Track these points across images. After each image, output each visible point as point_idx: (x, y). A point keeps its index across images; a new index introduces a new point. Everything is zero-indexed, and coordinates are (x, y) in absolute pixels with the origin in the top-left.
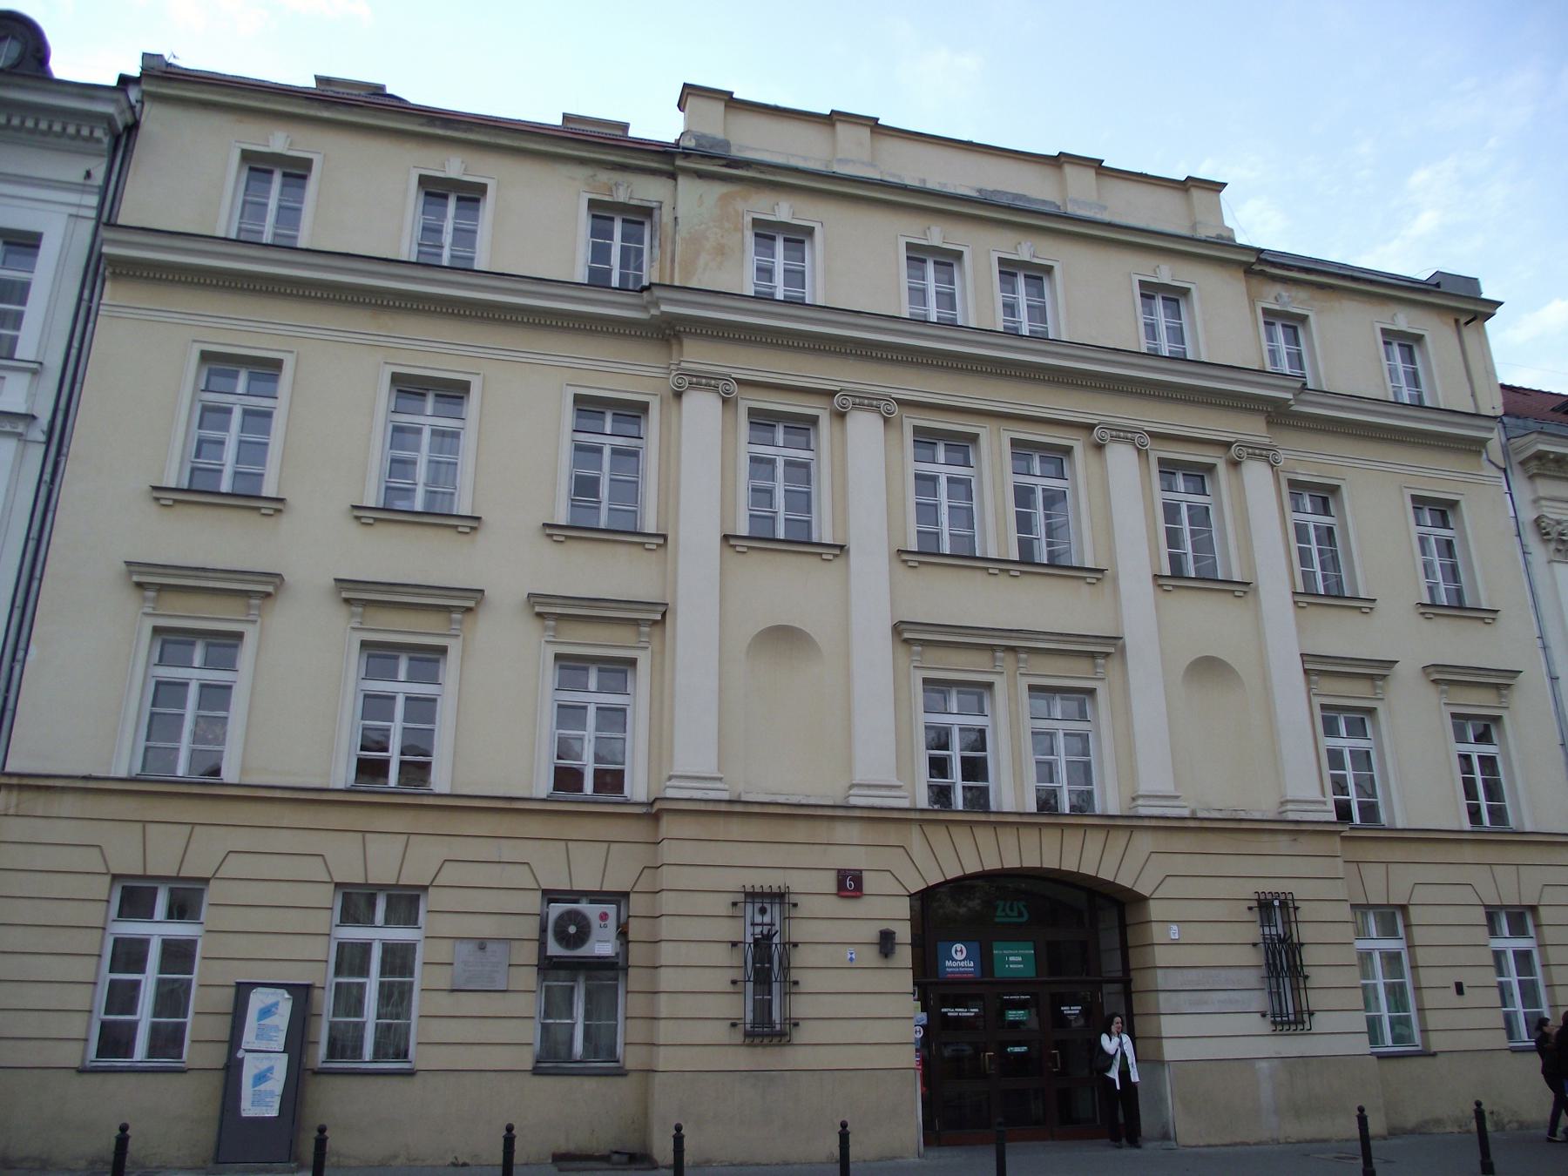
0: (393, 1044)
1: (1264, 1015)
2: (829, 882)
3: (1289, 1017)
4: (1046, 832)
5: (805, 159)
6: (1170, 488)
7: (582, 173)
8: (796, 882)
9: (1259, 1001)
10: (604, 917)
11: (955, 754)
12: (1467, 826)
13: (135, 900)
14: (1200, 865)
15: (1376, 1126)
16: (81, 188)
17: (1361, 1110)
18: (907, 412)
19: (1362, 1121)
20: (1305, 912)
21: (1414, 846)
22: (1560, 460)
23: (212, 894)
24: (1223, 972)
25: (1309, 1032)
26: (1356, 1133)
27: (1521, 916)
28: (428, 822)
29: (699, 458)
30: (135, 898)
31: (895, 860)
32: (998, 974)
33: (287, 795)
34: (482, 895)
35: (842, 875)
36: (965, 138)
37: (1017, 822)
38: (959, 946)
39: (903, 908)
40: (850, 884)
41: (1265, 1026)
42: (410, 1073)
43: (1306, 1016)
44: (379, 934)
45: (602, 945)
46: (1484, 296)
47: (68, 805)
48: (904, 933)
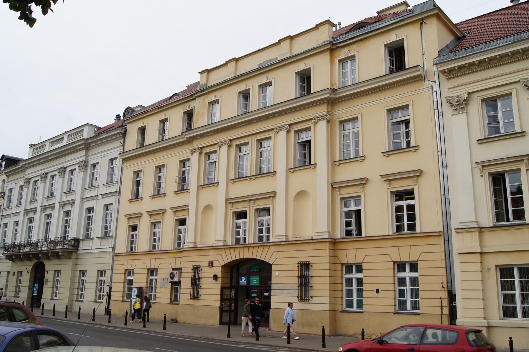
0: (360, 304)
1: (298, 297)
2: (207, 264)
3: (304, 298)
4: (250, 248)
5: (221, 78)
6: (98, 187)
8: (202, 264)
9: (297, 293)
11: (264, 228)
14: (286, 254)
17: (323, 327)
19: (323, 330)
20: (315, 267)
21: (431, 238)
23: (135, 271)
25: (309, 303)
26: (321, 333)
27: (130, 272)
28: (185, 254)
30: (401, 267)
31: (218, 258)
32: (251, 284)
33: (275, 244)
35: (209, 262)
36: (217, 65)
37: (250, 246)
38: (243, 278)
39: (220, 269)
40: (211, 264)
42: (419, 314)
43: (310, 298)
44: (408, 275)
45: (176, 279)
48: (219, 275)
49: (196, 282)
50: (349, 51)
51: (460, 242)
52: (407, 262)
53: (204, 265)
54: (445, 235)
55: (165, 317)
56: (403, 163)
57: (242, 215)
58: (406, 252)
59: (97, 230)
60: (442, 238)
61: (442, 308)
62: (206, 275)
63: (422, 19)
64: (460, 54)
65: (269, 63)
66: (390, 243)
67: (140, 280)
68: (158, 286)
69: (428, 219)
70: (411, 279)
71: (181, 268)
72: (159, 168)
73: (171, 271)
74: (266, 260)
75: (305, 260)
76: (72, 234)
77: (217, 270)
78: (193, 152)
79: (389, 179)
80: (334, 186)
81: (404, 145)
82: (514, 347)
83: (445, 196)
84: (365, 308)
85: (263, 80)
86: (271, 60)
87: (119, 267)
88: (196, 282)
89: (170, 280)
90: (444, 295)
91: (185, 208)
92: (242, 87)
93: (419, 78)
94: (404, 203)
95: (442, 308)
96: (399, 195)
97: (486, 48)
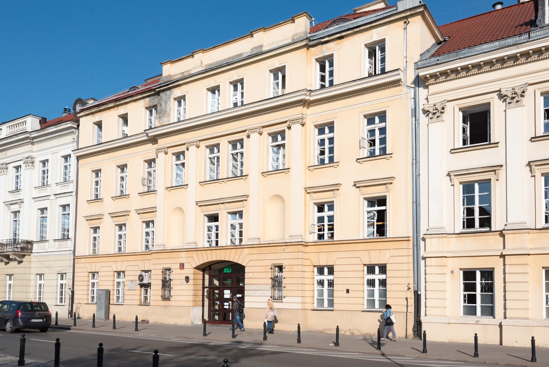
0: (331, 303)
14: (133, 263)
15: (139, 320)
18: (201, 142)
22: (548, 49)
24: (264, 286)
26: (297, 330)
35: (180, 264)
40: (182, 266)
41: (160, 298)
45: (145, 281)
49: (166, 284)
50: (328, 49)
51: (431, 247)
53: (175, 267)
54: (417, 239)
55: (137, 319)
57: (214, 218)
58: (379, 254)
59: (54, 231)
61: (407, 307)
62: (177, 277)
63: (406, 17)
64: (441, 58)
66: (361, 246)
67: (106, 282)
68: (126, 288)
69: (398, 223)
71: (150, 271)
72: (123, 168)
73: (139, 273)
74: (239, 262)
75: (278, 262)
76: (23, 236)
77: (189, 271)
78: (158, 150)
82: (479, 342)
84: (336, 307)
85: (234, 75)
86: (241, 55)
87: (80, 270)
88: (166, 284)
89: (139, 282)
91: (152, 210)
93: (396, 83)
95: (407, 307)
96: (372, 202)
97: (444, 59)
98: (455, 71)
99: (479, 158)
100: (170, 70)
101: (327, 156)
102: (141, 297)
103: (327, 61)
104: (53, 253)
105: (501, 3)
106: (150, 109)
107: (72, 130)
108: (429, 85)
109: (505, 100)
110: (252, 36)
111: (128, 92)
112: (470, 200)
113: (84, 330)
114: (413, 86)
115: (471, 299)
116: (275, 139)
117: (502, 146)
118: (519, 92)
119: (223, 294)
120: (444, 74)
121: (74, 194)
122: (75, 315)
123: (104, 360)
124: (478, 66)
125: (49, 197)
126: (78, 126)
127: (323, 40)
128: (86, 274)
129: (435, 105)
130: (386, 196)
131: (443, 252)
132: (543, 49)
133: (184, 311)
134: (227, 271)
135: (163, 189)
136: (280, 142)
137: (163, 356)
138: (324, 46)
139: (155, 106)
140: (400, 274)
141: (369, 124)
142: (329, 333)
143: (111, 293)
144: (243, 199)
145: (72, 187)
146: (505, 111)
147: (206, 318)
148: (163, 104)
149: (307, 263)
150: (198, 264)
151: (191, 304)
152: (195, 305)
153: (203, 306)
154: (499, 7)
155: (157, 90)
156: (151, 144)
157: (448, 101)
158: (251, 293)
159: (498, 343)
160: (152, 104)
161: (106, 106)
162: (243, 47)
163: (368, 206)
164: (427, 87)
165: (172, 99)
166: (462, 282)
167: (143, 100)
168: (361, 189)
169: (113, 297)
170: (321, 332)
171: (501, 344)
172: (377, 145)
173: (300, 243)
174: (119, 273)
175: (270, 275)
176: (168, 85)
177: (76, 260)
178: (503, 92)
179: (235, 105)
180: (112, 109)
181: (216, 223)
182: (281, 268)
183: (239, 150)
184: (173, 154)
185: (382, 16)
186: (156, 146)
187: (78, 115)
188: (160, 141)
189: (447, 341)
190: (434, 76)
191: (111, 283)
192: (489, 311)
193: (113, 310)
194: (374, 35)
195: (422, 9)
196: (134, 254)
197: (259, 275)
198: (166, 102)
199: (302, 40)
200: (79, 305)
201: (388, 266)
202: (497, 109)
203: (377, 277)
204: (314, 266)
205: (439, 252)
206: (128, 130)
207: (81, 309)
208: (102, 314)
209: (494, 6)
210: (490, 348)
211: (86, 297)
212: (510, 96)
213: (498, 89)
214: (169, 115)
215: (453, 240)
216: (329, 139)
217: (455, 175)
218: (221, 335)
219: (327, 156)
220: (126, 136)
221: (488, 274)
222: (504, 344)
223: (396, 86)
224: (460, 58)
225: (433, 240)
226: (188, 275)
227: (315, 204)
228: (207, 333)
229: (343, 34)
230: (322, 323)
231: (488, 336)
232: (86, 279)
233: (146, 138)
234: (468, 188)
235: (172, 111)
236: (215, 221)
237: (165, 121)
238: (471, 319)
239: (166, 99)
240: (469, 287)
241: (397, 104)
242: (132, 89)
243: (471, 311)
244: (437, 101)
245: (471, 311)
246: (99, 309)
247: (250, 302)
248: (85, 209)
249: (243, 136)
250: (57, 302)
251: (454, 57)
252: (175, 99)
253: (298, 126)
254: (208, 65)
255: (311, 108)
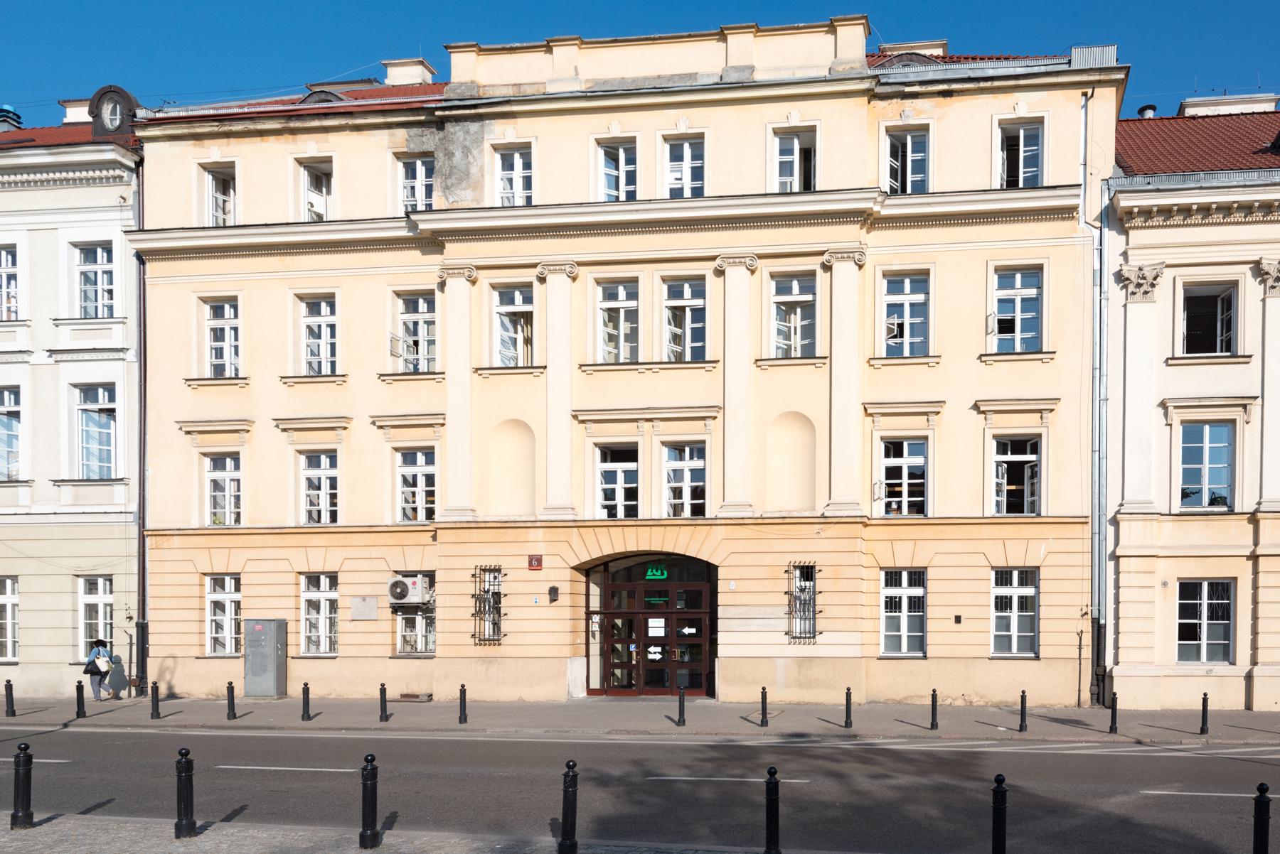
7: (384, 134)
8: (505, 563)
10: (414, 583)
12: (1088, 528)
13: (1003, 577)
14: (365, 552)
16: (121, 208)
24: (763, 609)
29: (468, 320)
30: (1003, 577)
34: (366, 576)
35: (531, 558)
40: (535, 562)
46: (1114, 89)
47: (176, 541)
49: (490, 605)
50: (920, 112)
51: (1133, 535)
52: (905, 568)
55: (383, 691)
56: (908, 382)
57: (626, 453)
58: (906, 548)
60: (1088, 528)
65: (688, 84)
66: (987, 531)
69: (1061, 486)
70: (910, 598)
73: (392, 579)
75: (806, 560)
77: (559, 572)
79: (285, 425)
80: (869, 411)
81: (326, 369)
82: (768, 700)
83: (1098, 453)
84: (341, 650)
86: (693, 76)
88: (490, 605)
90: (1087, 626)
92: (616, 125)
93: (1067, 213)
94: (619, 467)
96: (1008, 444)
98: (1186, 211)
99: (1211, 379)
100: (473, 70)
101: (908, 337)
102: (394, 638)
103: (621, 151)
104: (52, 518)
105: (1153, 108)
106: (408, 161)
107: (118, 172)
108: (1130, 228)
109: (1125, 287)
110: (549, 50)
111: (303, 101)
112: (1192, 455)
113: (289, 728)
114: (1098, 224)
115: (1189, 632)
116: (506, 298)
117: (1256, 361)
118: (1149, 275)
119: (647, 627)
120: (1166, 212)
121: (132, 355)
122: (155, 688)
123: (1008, 821)
124: (1226, 209)
125: (25, 357)
126: (140, 163)
127: (907, 89)
128: (195, 579)
129: (1140, 269)
130: (704, 442)
131: (1152, 547)
132: (1214, 206)
133: (545, 664)
134: (653, 574)
135: (468, 372)
136: (519, 306)
137: (791, 782)
138: (908, 102)
139: (427, 156)
140: (1068, 586)
141: (891, 291)
142: (918, 703)
143: (291, 628)
144: (707, 414)
145: (123, 335)
146: (1125, 306)
147: (595, 684)
148: (458, 154)
149: (866, 560)
150: (585, 558)
151: (566, 651)
152: (575, 655)
153: (587, 656)
154: (1149, 114)
155: (437, 113)
156: (417, 253)
157: (1168, 266)
158: (734, 624)
159: (1242, 706)
160: (416, 147)
161: (251, 126)
162: (697, 58)
163: (998, 453)
164: (1125, 232)
165: (487, 146)
166: (1178, 601)
167: (386, 132)
168: (588, 425)
169: (298, 638)
170: (899, 702)
171: (1249, 706)
172: (1018, 330)
173: (858, 520)
174: (313, 580)
175: (471, 589)
176: (475, 106)
177: (148, 540)
178: (1265, 266)
179: (676, 194)
180: (272, 138)
181: (630, 466)
182: (808, 572)
183: (622, 303)
184: (494, 287)
185: (1043, 69)
186: (435, 259)
187: (139, 133)
188: (451, 248)
189: (1158, 708)
190: (1147, 213)
191: (291, 603)
192: (1225, 653)
193: (299, 673)
194: (1024, 105)
195: (1121, 76)
196: (371, 530)
197: (756, 586)
198: (466, 151)
199: (863, 79)
200: (170, 662)
201: (340, 575)
202: (1250, 293)
203: (323, 594)
204: (205, 574)
205: (1137, 547)
206: (335, 205)
207: (178, 672)
208: (268, 682)
209: (1142, 111)
210: (1228, 717)
211: (195, 639)
212: (1135, 280)
213: (1257, 258)
214: (478, 186)
215: (1168, 525)
216: (694, 310)
217: (1176, 407)
218: (647, 722)
219: (908, 337)
220: (319, 219)
221: (1222, 589)
222: (1257, 707)
223: (1063, 219)
224: (1201, 188)
225: (1133, 523)
226: (556, 585)
227: (596, 444)
228: (312, 713)
229: (955, 86)
230: (907, 683)
231: (1227, 698)
232: (195, 591)
233: (404, 233)
234: (1192, 431)
235: (487, 177)
236: (895, 456)
237: (465, 197)
238: (1190, 667)
239: (467, 143)
240: (1188, 611)
241: (1071, 257)
242: (316, 97)
243: (1189, 653)
244: (1146, 263)
245: (1189, 653)
246: (253, 670)
247: (729, 642)
248: (173, 401)
249: (706, 269)
250: (76, 654)
251: (1179, 183)
252: (495, 148)
253: (743, 271)
254: (597, 82)
255: (874, 233)
